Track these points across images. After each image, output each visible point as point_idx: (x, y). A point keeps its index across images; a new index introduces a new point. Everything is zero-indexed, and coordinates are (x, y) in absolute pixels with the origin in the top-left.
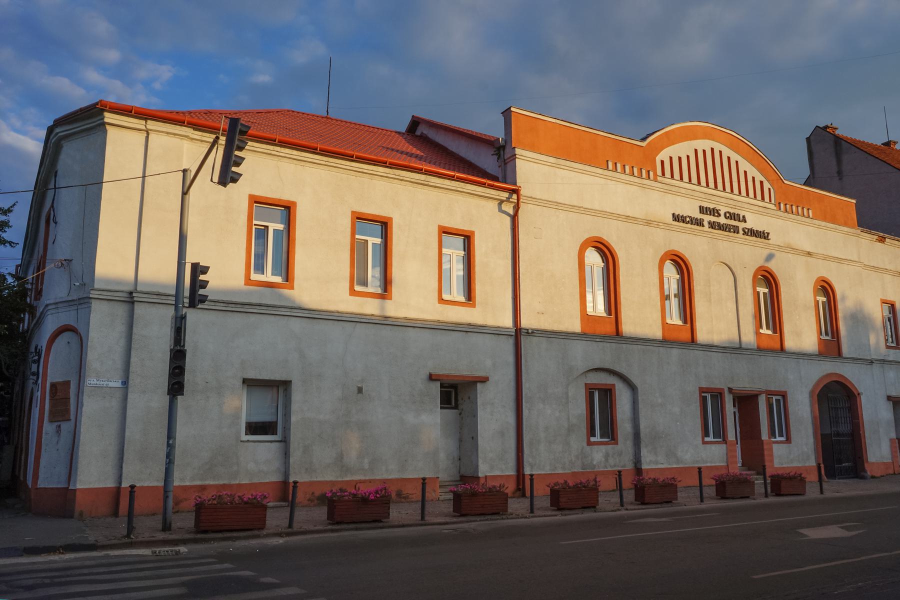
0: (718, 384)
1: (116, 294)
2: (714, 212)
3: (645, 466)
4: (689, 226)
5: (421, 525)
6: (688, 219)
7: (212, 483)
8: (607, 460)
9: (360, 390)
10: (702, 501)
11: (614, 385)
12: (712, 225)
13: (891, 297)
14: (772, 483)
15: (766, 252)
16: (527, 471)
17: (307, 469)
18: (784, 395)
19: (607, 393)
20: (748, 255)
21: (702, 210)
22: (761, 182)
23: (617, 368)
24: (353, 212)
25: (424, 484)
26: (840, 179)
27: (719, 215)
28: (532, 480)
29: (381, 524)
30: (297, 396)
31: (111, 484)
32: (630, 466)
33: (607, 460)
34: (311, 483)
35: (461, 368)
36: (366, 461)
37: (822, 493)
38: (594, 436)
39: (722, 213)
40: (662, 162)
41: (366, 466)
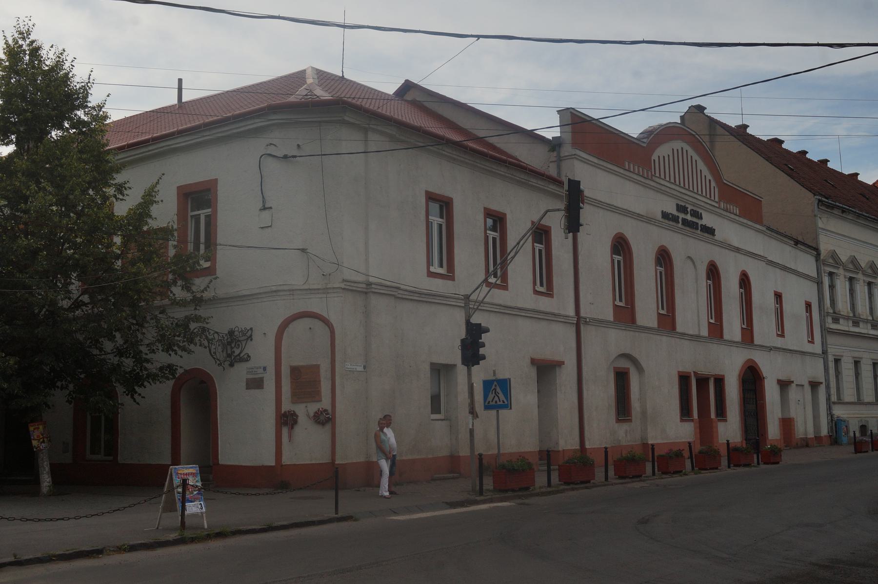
3: (587, 446)
4: (671, 223)
5: (549, 493)
11: (628, 369)
13: (779, 290)
24: (485, 209)
28: (653, 449)
29: (588, 485)
31: (326, 459)
35: (547, 353)
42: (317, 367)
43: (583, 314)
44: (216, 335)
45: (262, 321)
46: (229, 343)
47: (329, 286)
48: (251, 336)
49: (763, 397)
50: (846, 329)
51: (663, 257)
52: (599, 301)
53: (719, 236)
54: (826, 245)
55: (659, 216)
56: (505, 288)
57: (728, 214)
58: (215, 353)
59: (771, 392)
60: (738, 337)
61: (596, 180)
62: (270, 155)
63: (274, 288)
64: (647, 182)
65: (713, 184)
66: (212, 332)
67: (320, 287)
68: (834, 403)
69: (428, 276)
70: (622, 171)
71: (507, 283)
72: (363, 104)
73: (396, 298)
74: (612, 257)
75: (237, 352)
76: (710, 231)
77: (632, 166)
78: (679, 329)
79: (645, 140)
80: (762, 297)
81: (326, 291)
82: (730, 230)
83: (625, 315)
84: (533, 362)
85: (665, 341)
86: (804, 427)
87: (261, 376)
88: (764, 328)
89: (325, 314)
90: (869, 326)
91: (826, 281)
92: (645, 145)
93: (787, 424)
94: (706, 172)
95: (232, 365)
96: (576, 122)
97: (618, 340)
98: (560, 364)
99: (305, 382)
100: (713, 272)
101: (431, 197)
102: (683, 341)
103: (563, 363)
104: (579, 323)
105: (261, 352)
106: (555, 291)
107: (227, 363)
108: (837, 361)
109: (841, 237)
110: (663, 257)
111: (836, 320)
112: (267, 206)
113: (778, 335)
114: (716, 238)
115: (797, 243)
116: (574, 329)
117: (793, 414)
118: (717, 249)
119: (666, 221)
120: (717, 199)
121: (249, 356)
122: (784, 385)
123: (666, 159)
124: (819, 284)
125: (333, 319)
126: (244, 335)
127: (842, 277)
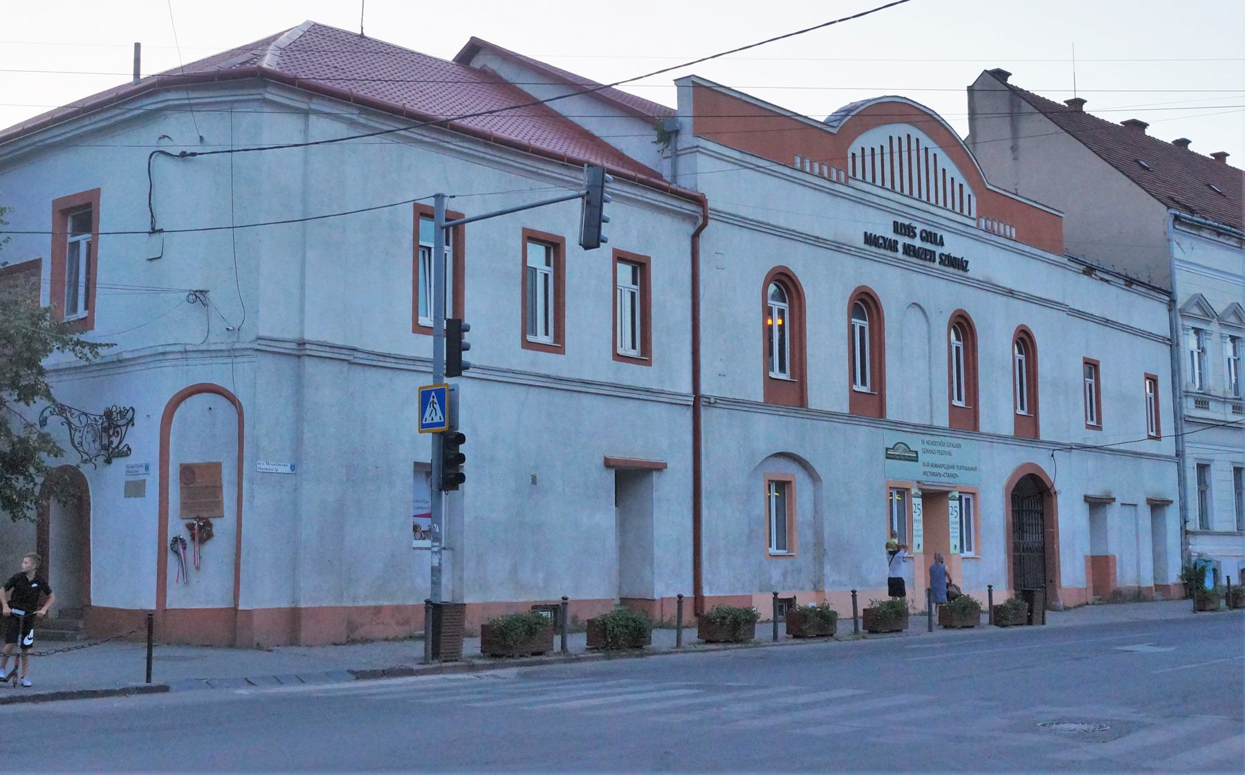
1: (279, 344)
2: (908, 231)
4: (882, 251)
6: (881, 241)
7: (386, 603)
8: (785, 579)
9: (534, 480)
10: (930, 629)
12: (908, 250)
14: (864, 617)
16: (706, 592)
17: (481, 586)
19: (782, 486)
20: (944, 295)
21: (898, 228)
22: (961, 186)
23: (801, 453)
24: (525, 230)
26: (1015, 159)
27: (915, 235)
29: (544, 658)
32: (688, 593)
33: (785, 579)
34: (486, 606)
35: (636, 451)
36: (541, 575)
39: (918, 231)
40: (854, 155)
41: (541, 585)
42: (217, 466)
43: (704, 390)
44: (83, 418)
45: (147, 395)
46: (106, 430)
47: (237, 346)
48: (132, 419)
49: (1053, 523)
50: (1222, 418)
51: (865, 304)
52: (738, 368)
53: (974, 271)
54: (1185, 288)
55: (860, 241)
56: (648, 363)
57: (994, 238)
58: (81, 444)
59: (1070, 517)
60: (1008, 428)
61: (715, 174)
62: (162, 152)
63: (161, 350)
64: (838, 187)
65: (967, 190)
66: (77, 413)
67: (223, 347)
68: (1194, 533)
69: (414, 331)
70: (787, 171)
71: (563, 345)
72: (408, 106)
73: (350, 363)
74: (849, 321)
75: (116, 441)
76: (959, 264)
77: (834, 171)
78: (892, 413)
79: (835, 124)
80: (1058, 365)
81: (232, 353)
82: (992, 261)
83: (788, 392)
84: (608, 464)
85: (864, 437)
86: (1134, 569)
87: (141, 477)
88: (1060, 414)
89: (231, 390)
90: (1229, 408)
91: (1189, 342)
92: (834, 131)
93: (1100, 566)
94: (953, 171)
95: (108, 461)
96: (699, 91)
97: (773, 431)
98: (660, 468)
99: (201, 488)
100: (962, 325)
101: (1148, 377)
102: (880, 431)
103: (665, 466)
104: (698, 403)
105: (142, 440)
106: (654, 355)
107: (101, 459)
108: (1203, 468)
109: (1204, 267)
110: (865, 304)
111: (1202, 403)
112: (157, 228)
113: (1089, 427)
114: (969, 274)
115: (1130, 282)
116: (689, 413)
117: (1113, 549)
118: (970, 291)
119: (873, 249)
120: (974, 215)
121: (129, 449)
122: (1097, 504)
123: (878, 151)
124: (1173, 343)
125: (242, 398)
126: (123, 417)
127: (1215, 338)
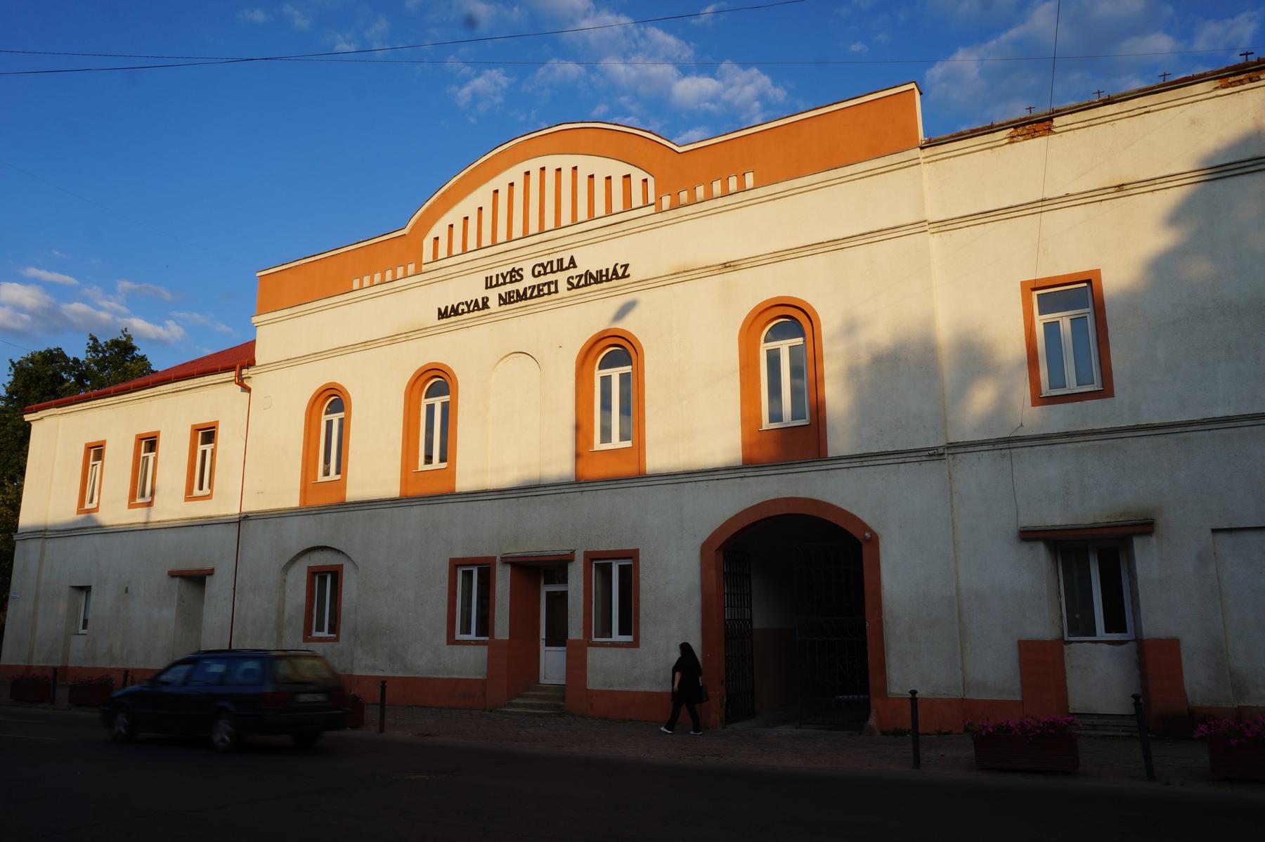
0: (483, 551)
9: (127, 591)
11: (341, 566)
12: (505, 300)
15: (617, 303)
18: (633, 555)
25: (383, 688)
30: (93, 597)
35: (194, 563)
37: (382, 731)
38: (320, 629)
